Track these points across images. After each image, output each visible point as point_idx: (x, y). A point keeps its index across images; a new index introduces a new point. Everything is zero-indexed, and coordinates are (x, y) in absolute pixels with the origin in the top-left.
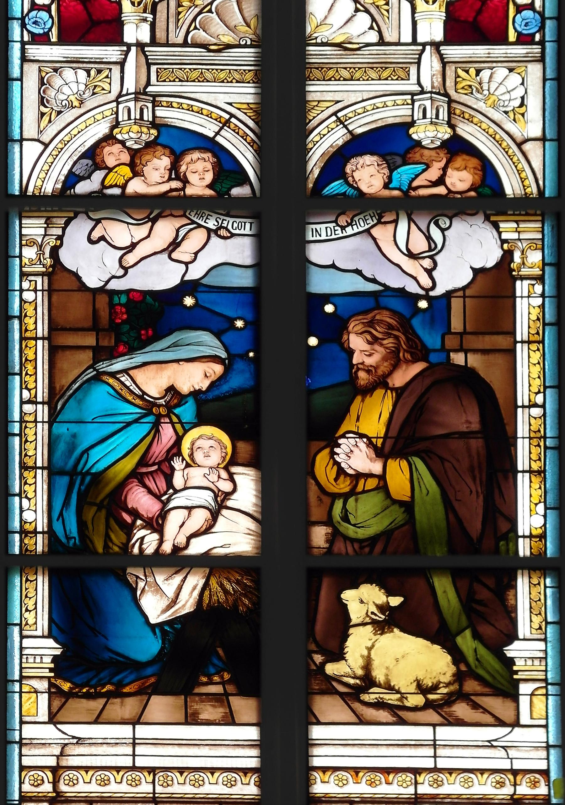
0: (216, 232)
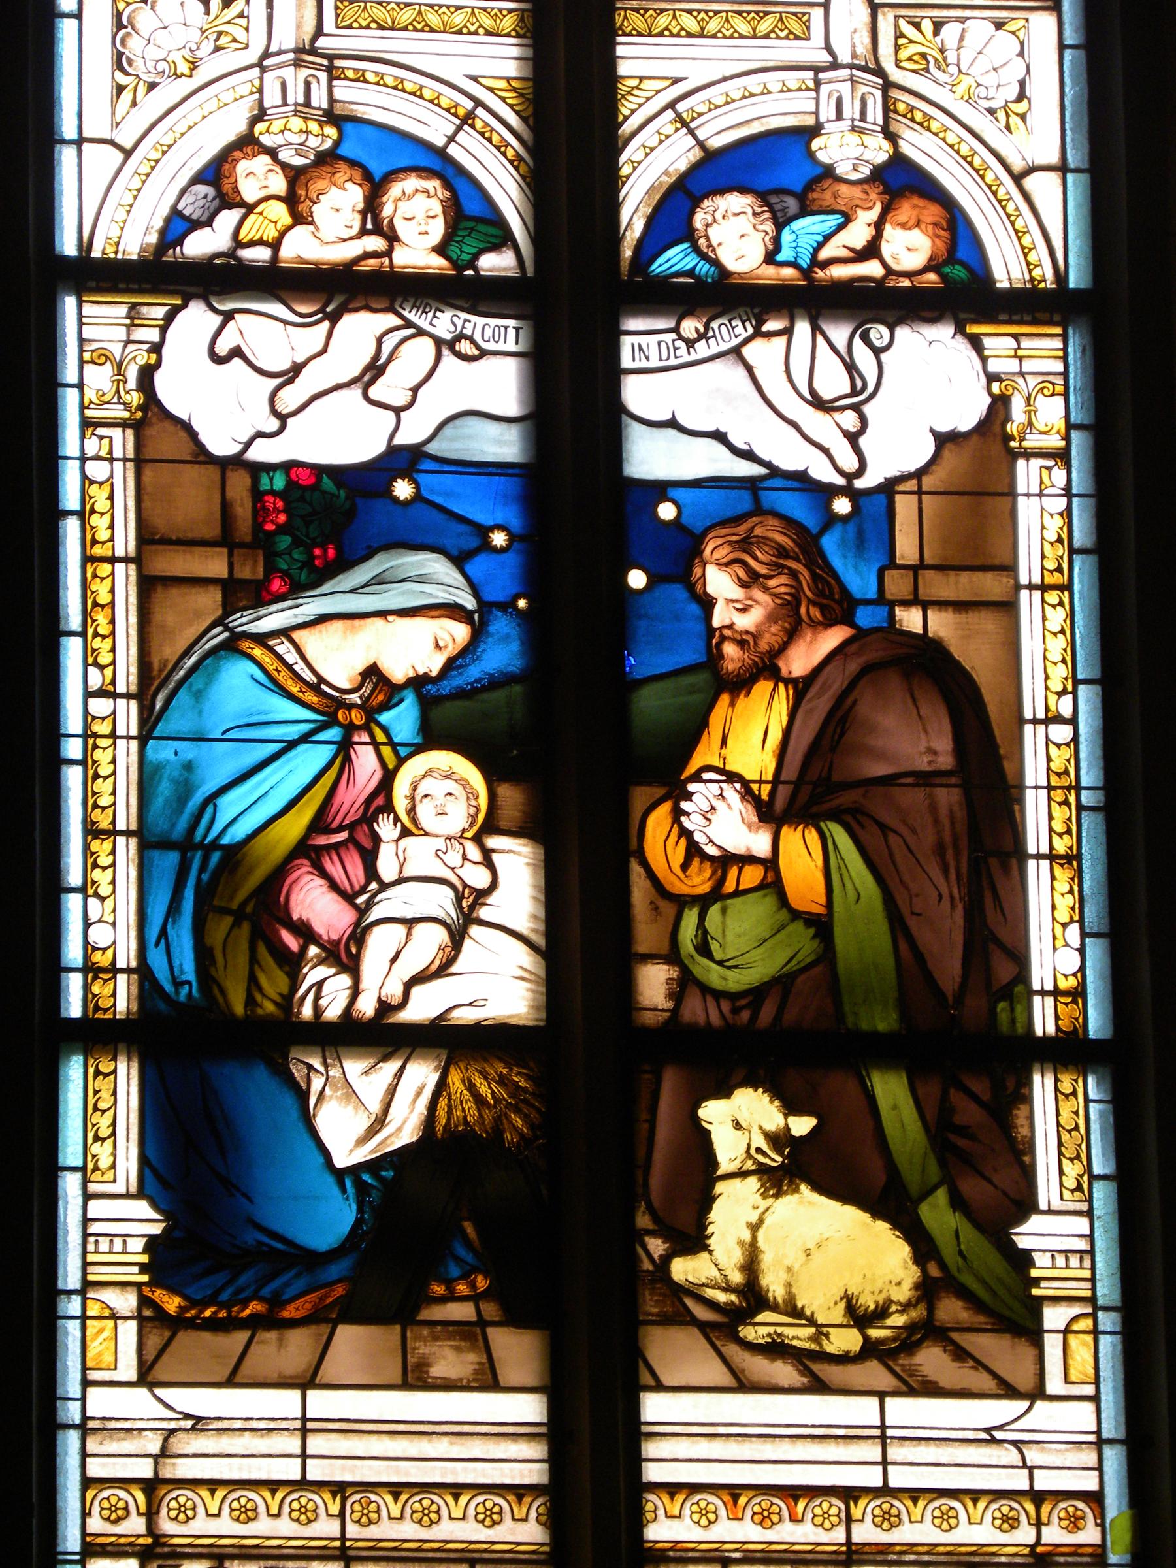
0: (451, 345)
